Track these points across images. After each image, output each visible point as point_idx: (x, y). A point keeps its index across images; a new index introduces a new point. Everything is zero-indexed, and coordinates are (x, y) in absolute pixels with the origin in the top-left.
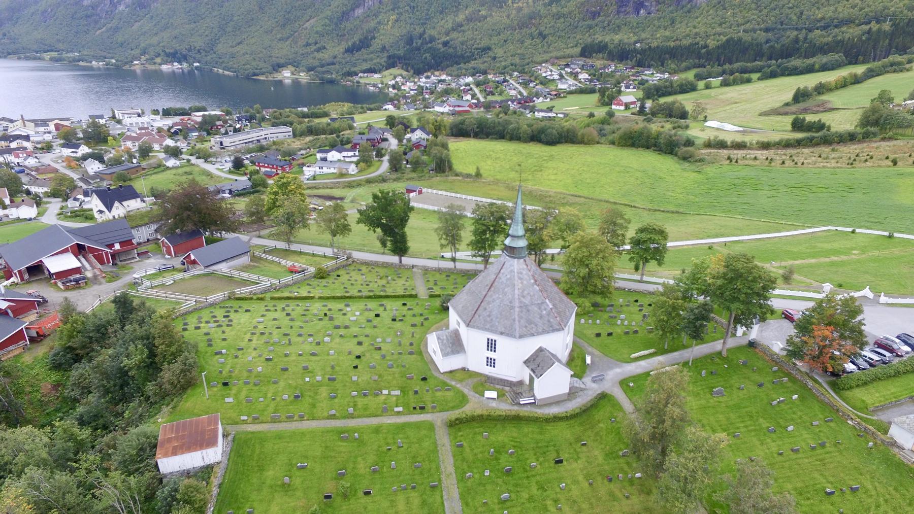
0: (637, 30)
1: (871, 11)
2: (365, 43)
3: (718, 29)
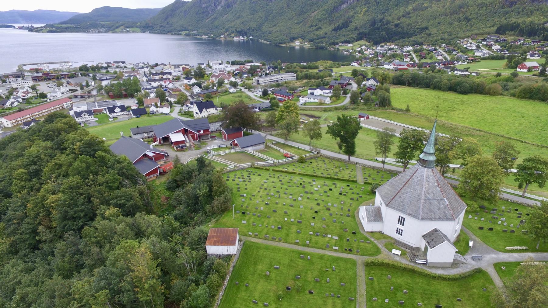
2: (345, 25)
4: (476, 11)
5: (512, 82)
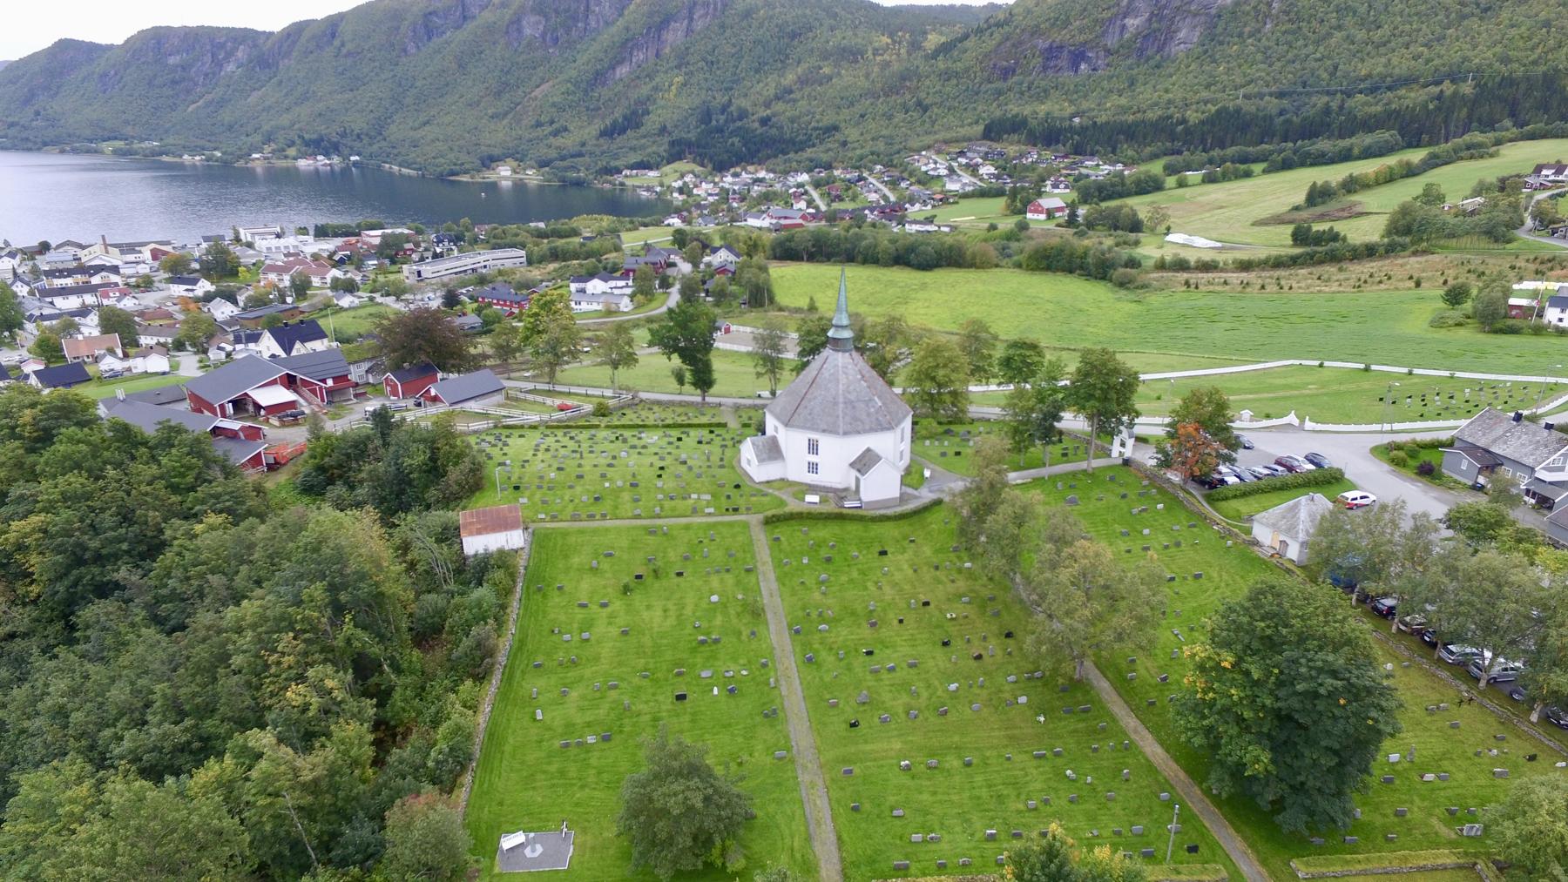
0: (1075, 96)
1: (1444, 65)
2: (632, 121)
3: (1204, 94)
4: (937, 88)
5: (1018, 240)
